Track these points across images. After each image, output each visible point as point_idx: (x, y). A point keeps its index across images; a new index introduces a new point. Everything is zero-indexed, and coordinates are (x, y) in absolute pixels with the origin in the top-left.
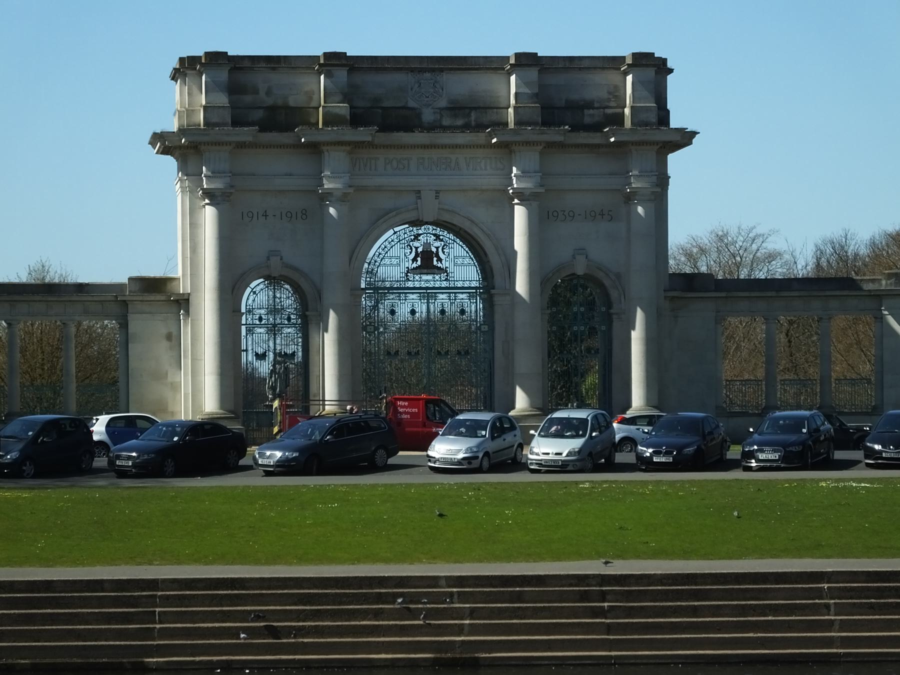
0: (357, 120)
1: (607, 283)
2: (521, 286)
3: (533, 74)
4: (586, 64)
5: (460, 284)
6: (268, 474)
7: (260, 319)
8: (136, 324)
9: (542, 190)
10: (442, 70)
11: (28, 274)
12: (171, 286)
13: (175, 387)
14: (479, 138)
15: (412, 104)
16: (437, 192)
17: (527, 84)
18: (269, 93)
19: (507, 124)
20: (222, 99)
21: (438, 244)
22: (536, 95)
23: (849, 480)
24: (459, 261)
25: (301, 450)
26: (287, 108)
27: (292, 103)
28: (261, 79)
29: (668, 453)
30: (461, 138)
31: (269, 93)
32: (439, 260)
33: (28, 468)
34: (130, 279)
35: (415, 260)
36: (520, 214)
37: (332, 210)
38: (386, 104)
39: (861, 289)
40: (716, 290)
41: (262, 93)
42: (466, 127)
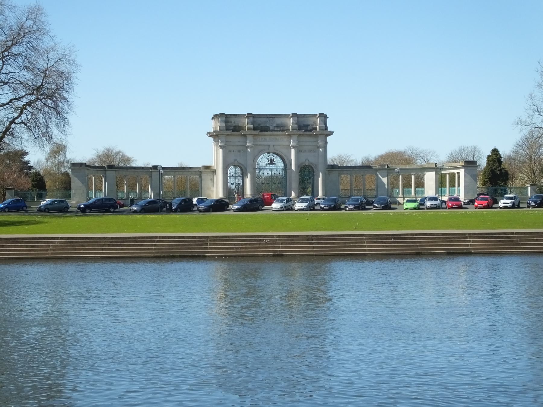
0: (255, 129)
3: (296, 118)
4: (308, 116)
5: (279, 167)
7: (232, 175)
9: (298, 145)
10: (275, 117)
12: (211, 168)
13: (213, 191)
14: (283, 133)
15: (267, 125)
17: (294, 121)
18: (234, 123)
20: (224, 124)
21: (274, 158)
22: (296, 123)
24: (279, 162)
25: (242, 206)
27: (240, 125)
28: (233, 120)
32: (274, 161)
33: (47, 210)
34: (202, 166)
35: (268, 161)
36: (293, 151)
37: (249, 150)
38: (261, 125)
39: (372, 168)
41: (233, 123)
42: (280, 130)
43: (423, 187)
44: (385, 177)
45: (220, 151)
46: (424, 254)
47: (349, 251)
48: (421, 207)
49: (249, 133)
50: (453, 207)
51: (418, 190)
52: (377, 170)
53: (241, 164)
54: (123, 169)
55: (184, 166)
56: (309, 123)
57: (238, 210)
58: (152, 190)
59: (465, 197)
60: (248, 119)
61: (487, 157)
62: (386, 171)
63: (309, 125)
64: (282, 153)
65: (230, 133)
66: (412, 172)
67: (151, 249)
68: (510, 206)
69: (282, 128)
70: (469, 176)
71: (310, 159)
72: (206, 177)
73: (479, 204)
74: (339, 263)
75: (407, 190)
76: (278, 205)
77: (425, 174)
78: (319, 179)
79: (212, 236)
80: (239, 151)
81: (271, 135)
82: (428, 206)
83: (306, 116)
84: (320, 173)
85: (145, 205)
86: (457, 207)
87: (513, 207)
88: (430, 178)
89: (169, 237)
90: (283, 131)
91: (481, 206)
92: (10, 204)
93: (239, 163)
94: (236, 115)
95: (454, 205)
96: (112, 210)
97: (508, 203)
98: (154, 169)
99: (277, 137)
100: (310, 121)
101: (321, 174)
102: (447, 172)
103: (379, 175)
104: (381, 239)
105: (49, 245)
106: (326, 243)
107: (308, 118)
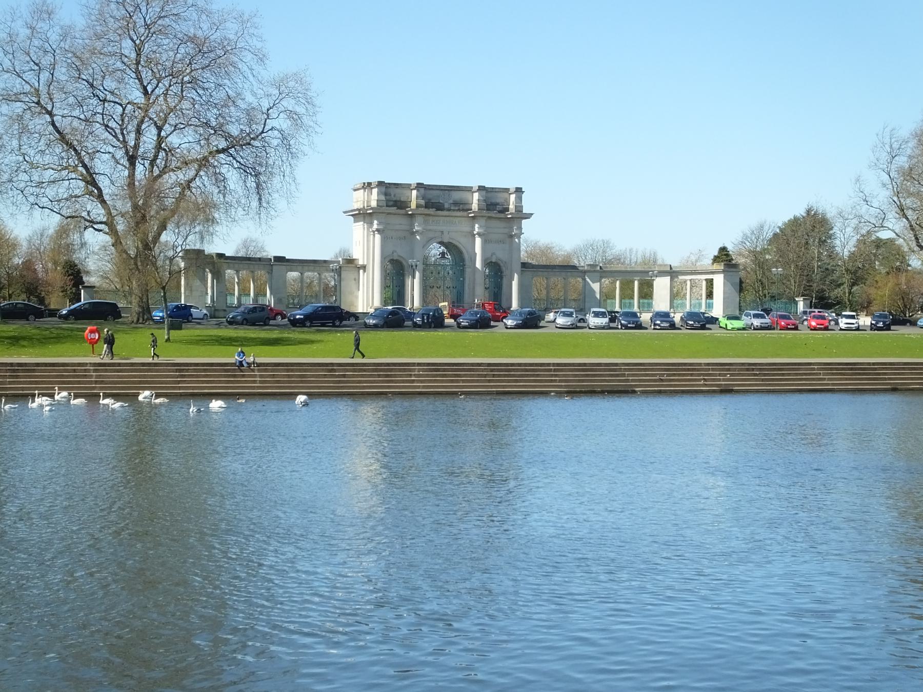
0: (427, 206)
1: (502, 265)
2: (478, 264)
3: (484, 193)
4: (497, 190)
6: (232, 322)
8: (343, 274)
9: (486, 233)
10: (451, 190)
11: (669, 263)
12: (356, 262)
13: (357, 297)
14: (465, 214)
15: (441, 201)
16: (449, 232)
17: (482, 196)
18: (395, 196)
19: (507, 209)
20: (383, 198)
22: (485, 200)
23: (718, 333)
25: (522, 320)
26: (400, 201)
27: (402, 200)
28: (392, 191)
29: (633, 324)
30: (459, 214)
31: (395, 196)
33: (245, 322)
36: (478, 241)
37: (418, 237)
38: (432, 201)
39: (578, 269)
40: (532, 268)
41: (392, 196)
42: (459, 210)
43: (651, 298)
44: (597, 282)
45: (378, 237)
46: (901, 390)
47: (799, 385)
48: (612, 325)
49: (419, 212)
50: (789, 327)
51: (643, 303)
52: (585, 272)
53: (402, 257)
54: (235, 260)
55: (252, 255)
56: (498, 201)
57: (517, 327)
58: (271, 294)
59: (723, 313)
60: (418, 191)
61: (712, 258)
62: (598, 274)
63: (498, 204)
64: (460, 243)
65: (393, 211)
66: (635, 277)
67: (555, 381)
68: (856, 327)
69: (461, 206)
70: (729, 284)
71: (500, 254)
72: (347, 275)
73: (818, 324)
74: (531, 403)
75: (627, 301)
76: (567, 320)
77: (654, 280)
78: (513, 282)
79: (623, 363)
80: (400, 239)
81: (445, 216)
82: (757, 326)
83: (494, 190)
84: (515, 274)
85: (388, 317)
86: (793, 327)
87: (573, 327)
88: (662, 286)
89: (565, 365)
90: (463, 210)
91: (821, 326)
92: (173, 311)
93: (399, 256)
94: (397, 184)
95: (789, 325)
96: (338, 324)
97: (853, 324)
98: (275, 261)
99: (457, 220)
100: (500, 198)
101: (516, 276)
102: (688, 277)
103: (588, 280)
104: (837, 369)
105: (411, 375)
106: (774, 375)
107: (496, 194)
